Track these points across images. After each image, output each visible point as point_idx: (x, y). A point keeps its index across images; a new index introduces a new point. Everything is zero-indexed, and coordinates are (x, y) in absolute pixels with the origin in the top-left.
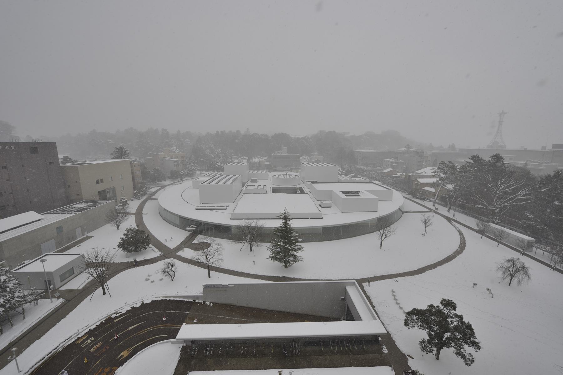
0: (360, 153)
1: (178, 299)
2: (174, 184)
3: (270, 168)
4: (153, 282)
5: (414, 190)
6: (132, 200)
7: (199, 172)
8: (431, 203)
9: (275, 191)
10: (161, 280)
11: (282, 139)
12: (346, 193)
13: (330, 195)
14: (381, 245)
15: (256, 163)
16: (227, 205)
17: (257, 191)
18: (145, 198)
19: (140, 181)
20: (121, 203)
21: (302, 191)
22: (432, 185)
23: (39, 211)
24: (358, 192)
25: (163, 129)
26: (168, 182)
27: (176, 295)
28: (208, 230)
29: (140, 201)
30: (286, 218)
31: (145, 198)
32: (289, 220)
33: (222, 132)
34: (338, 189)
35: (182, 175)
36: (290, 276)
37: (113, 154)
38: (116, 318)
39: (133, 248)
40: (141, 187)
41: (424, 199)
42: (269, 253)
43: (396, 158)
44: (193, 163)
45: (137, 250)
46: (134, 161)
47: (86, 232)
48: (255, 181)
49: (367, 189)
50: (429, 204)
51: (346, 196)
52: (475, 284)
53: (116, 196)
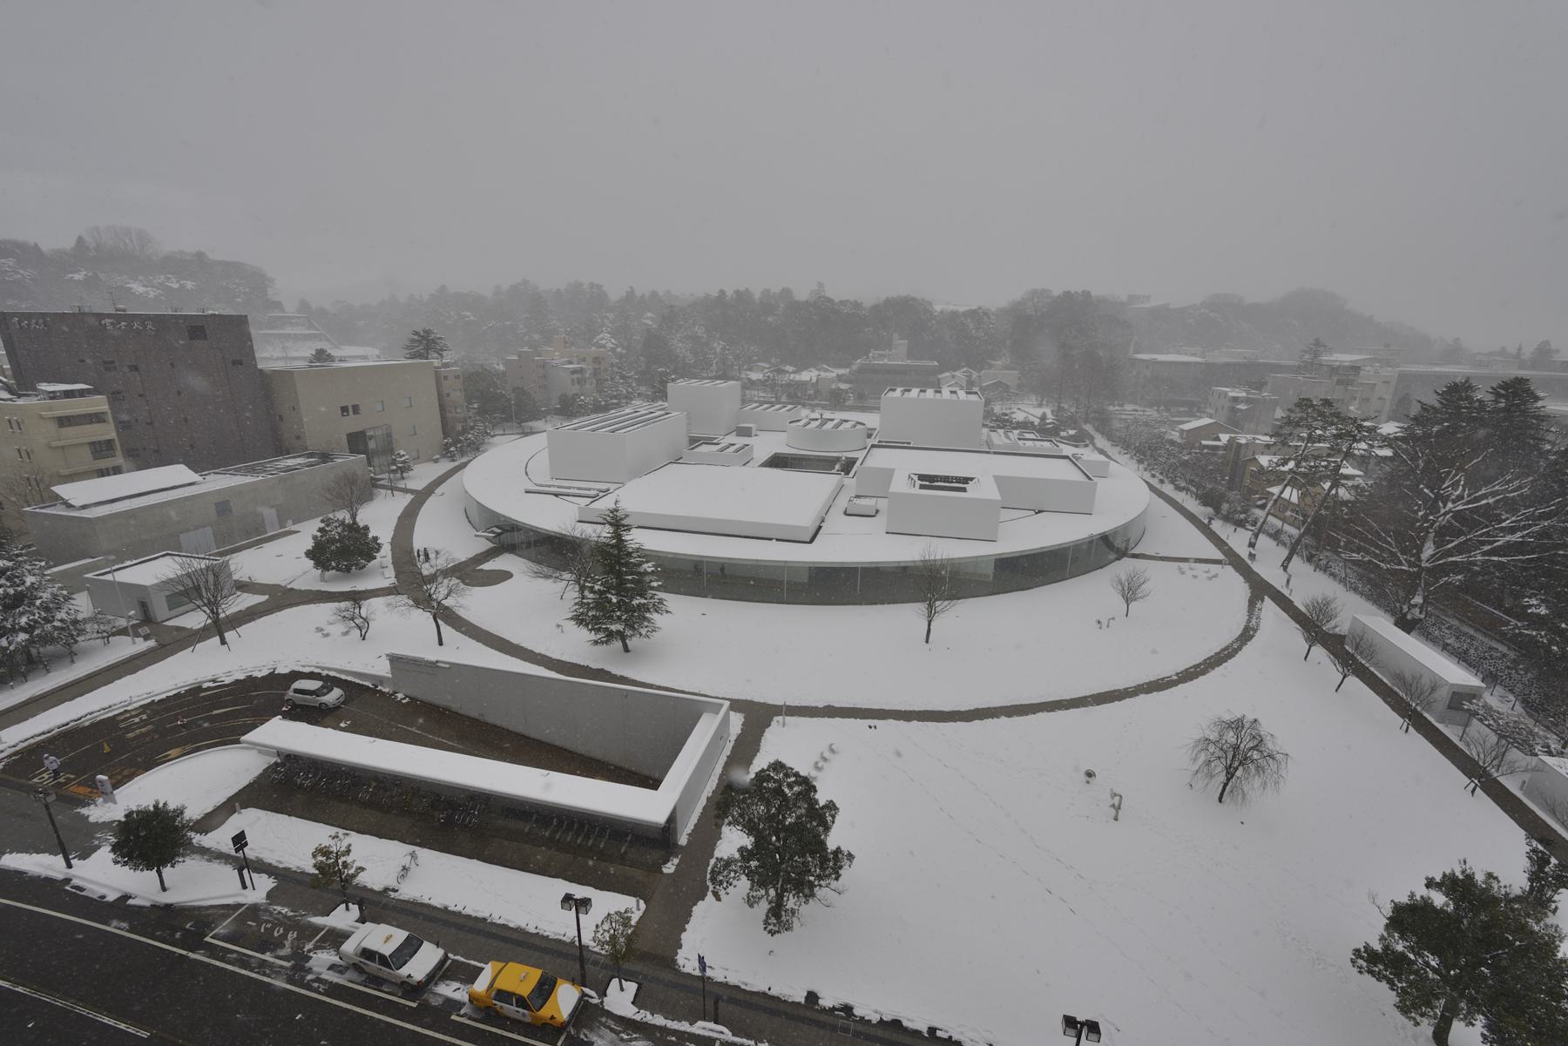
4: (327, 635)
6: (436, 461)
11: (904, 315)
12: (929, 481)
16: (604, 486)
23: (196, 467)
24: (966, 480)
28: (529, 545)
29: (450, 465)
30: (617, 523)
32: (628, 528)
38: (209, 689)
40: (465, 431)
44: (623, 377)
46: (446, 365)
48: (745, 432)
50: (1238, 540)
52: (1090, 774)
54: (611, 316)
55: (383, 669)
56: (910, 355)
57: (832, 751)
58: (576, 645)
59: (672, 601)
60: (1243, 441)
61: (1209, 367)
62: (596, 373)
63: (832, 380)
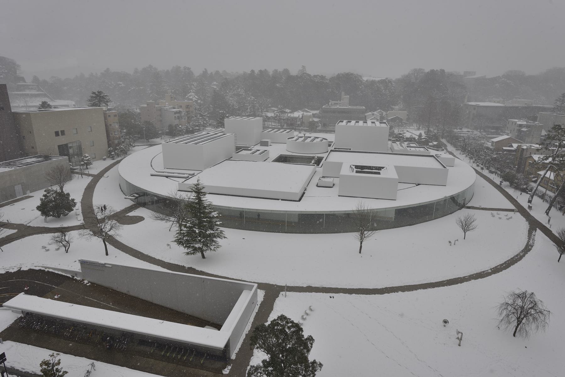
0: (475, 107)
1: (56, 272)
4: (48, 250)
6: (104, 159)
9: (283, 159)
12: (361, 169)
14: (361, 247)
16: (192, 172)
24: (380, 168)
28: (153, 203)
30: (199, 191)
32: (205, 194)
33: (185, 68)
36: (198, 268)
37: (90, 100)
40: (119, 144)
44: (201, 115)
46: (109, 110)
47: (29, 191)
48: (265, 144)
50: (523, 199)
52: (446, 322)
54: (195, 84)
55: (77, 268)
57: (311, 310)
58: (177, 255)
59: (227, 231)
60: (525, 147)
61: (505, 107)
63: (310, 117)
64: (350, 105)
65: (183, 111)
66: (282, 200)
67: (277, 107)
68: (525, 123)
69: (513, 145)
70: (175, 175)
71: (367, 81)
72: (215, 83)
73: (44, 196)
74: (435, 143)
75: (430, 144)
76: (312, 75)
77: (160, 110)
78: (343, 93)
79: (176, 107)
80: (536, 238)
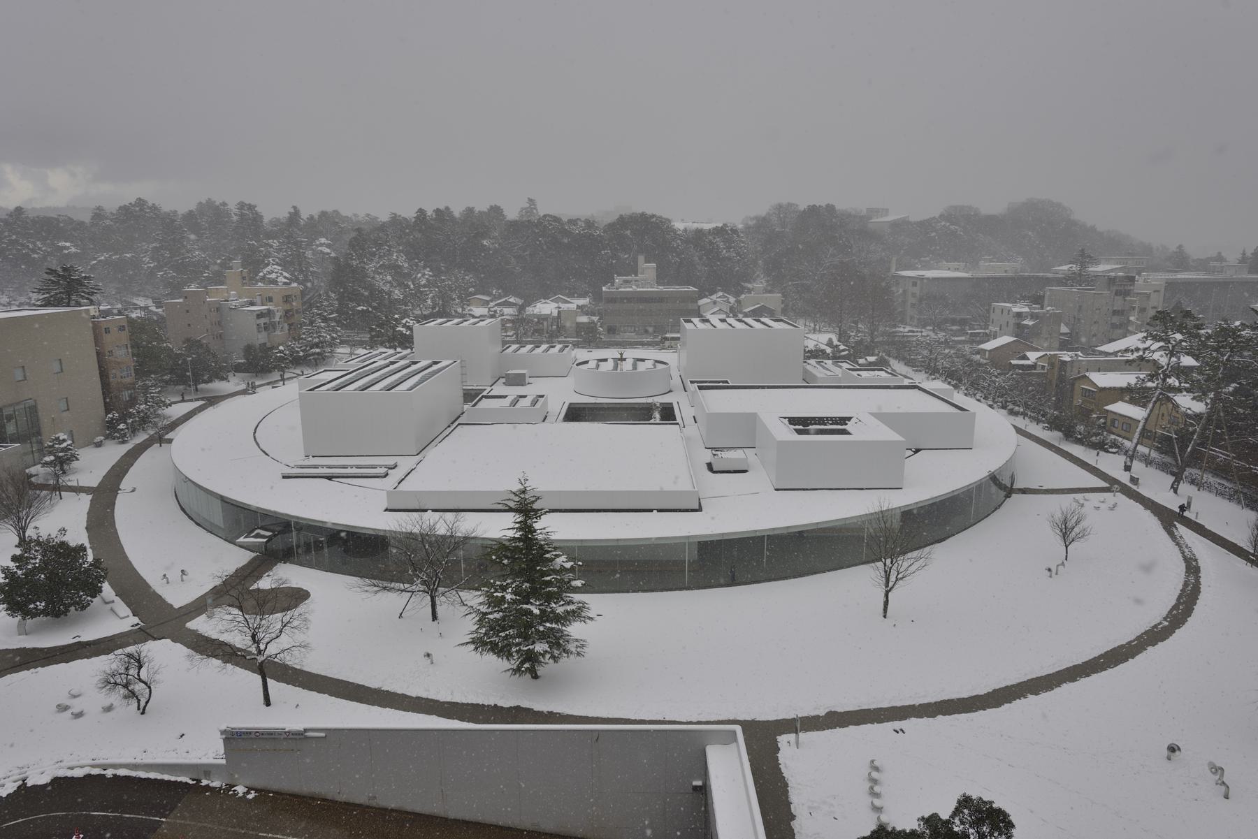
0: (915, 281)
1: (143, 775)
2: (250, 390)
3: (588, 337)
4: (79, 715)
5: (1066, 411)
6: (99, 445)
7: (347, 350)
8: (1121, 460)
9: (575, 414)
10: (109, 709)
11: (643, 234)
12: (802, 424)
13: (749, 425)
14: (886, 603)
15: (542, 318)
16: (390, 461)
17: (511, 417)
18: (141, 437)
19: (128, 380)
20: (50, 453)
21: (668, 414)
22: (1134, 395)
24: (844, 420)
25: (242, 205)
26: (234, 383)
27: (138, 761)
28: (308, 549)
29: (124, 449)
30: (526, 508)
31: (141, 437)
32: (537, 514)
33: (828, 205)
34: (773, 408)
35: (282, 359)
36: (537, 707)
39: (41, 605)
40: (133, 401)
41: (1101, 447)
42: (468, 626)
43: (1038, 300)
44: (325, 320)
45: (57, 612)
46: (106, 314)
48: (518, 380)
49: (872, 407)
50: (1112, 464)
51: (799, 432)
52: (1173, 749)
53: (39, 433)
54: (275, 243)
55: (210, 751)
56: (660, 279)
57: (877, 769)
58: (480, 678)
59: (595, 602)
60: (1068, 359)
61: (976, 282)
62: (288, 314)
63: (575, 314)
64: (659, 284)
65: (278, 309)
66: (434, 511)
67: (489, 294)
68: (1027, 309)
69: (1029, 354)
70: (349, 471)
71: (685, 230)
72: (323, 240)
73: (14, 558)
74: (872, 359)
75: (861, 361)
76: (565, 219)
77: (218, 309)
78: (641, 258)
79: (258, 300)
80: (1187, 541)
